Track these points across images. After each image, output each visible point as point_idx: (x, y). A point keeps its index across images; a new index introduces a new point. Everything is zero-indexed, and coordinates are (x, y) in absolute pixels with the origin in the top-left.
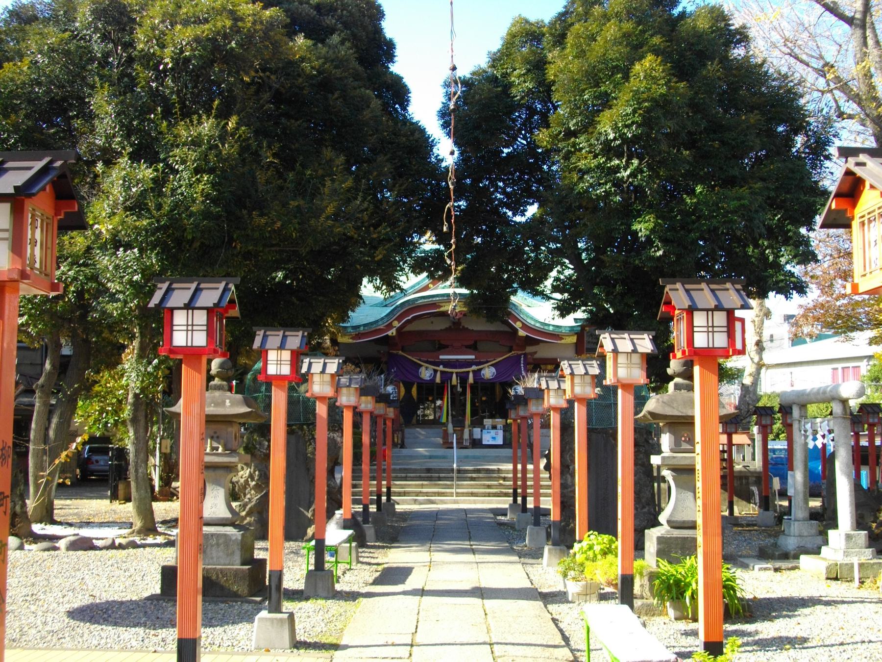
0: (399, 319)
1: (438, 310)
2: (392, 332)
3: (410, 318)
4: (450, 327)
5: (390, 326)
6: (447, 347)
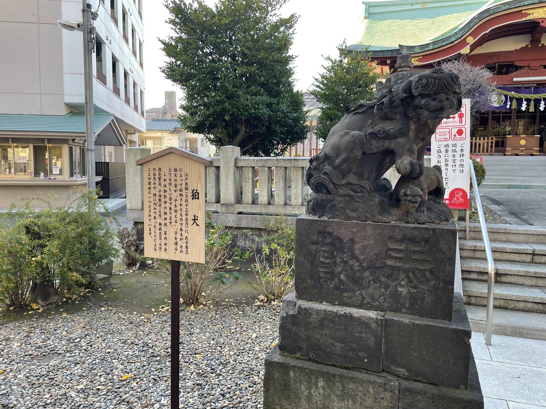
0: (473, 34)
1: (524, 19)
2: (466, 51)
3: (488, 32)
4: (527, 46)
5: (463, 43)
6: (521, 67)
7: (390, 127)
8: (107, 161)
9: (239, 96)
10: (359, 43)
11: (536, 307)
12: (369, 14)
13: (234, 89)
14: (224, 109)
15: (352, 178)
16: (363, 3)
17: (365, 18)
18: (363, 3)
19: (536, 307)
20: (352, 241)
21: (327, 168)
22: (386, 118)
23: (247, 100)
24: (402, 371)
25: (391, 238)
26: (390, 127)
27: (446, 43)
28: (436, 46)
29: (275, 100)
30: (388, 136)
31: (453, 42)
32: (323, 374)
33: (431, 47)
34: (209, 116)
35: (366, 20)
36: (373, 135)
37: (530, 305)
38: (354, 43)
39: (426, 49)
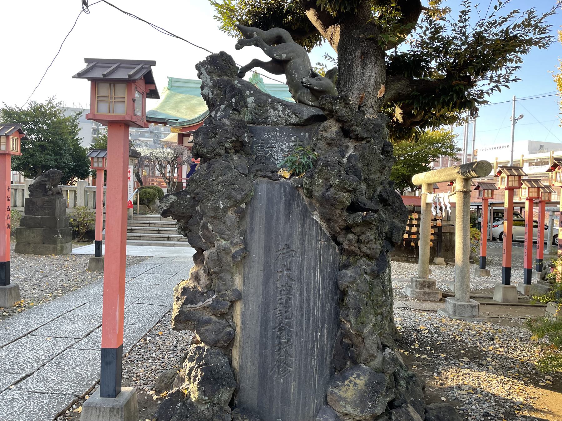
7: (46, 179)
8: (341, 256)
9: (36, 156)
10: (156, 110)
11: (137, 238)
12: (172, 86)
13: (34, 152)
14: (28, 162)
15: (38, 190)
16: (168, 77)
17: (168, 89)
18: (168, 77)
19: (137, 238)
20: (37, 202)
21: (32, 187)
22: (45, 177)
23: (41, 157)
24: (45, 227)
25: (44, 201)
26: (46, 179)
27: (194, 122)
28: (188, 124)
29: (58, 157)
30: (45, 181)
31: (198, 122)
32: (29, 229)
33: (186, 124)
34: (20, 164)
35: (168, 91)
36: (42, 181)
37: (136, 238)
38: (153, 109)
39: (183, 124)
